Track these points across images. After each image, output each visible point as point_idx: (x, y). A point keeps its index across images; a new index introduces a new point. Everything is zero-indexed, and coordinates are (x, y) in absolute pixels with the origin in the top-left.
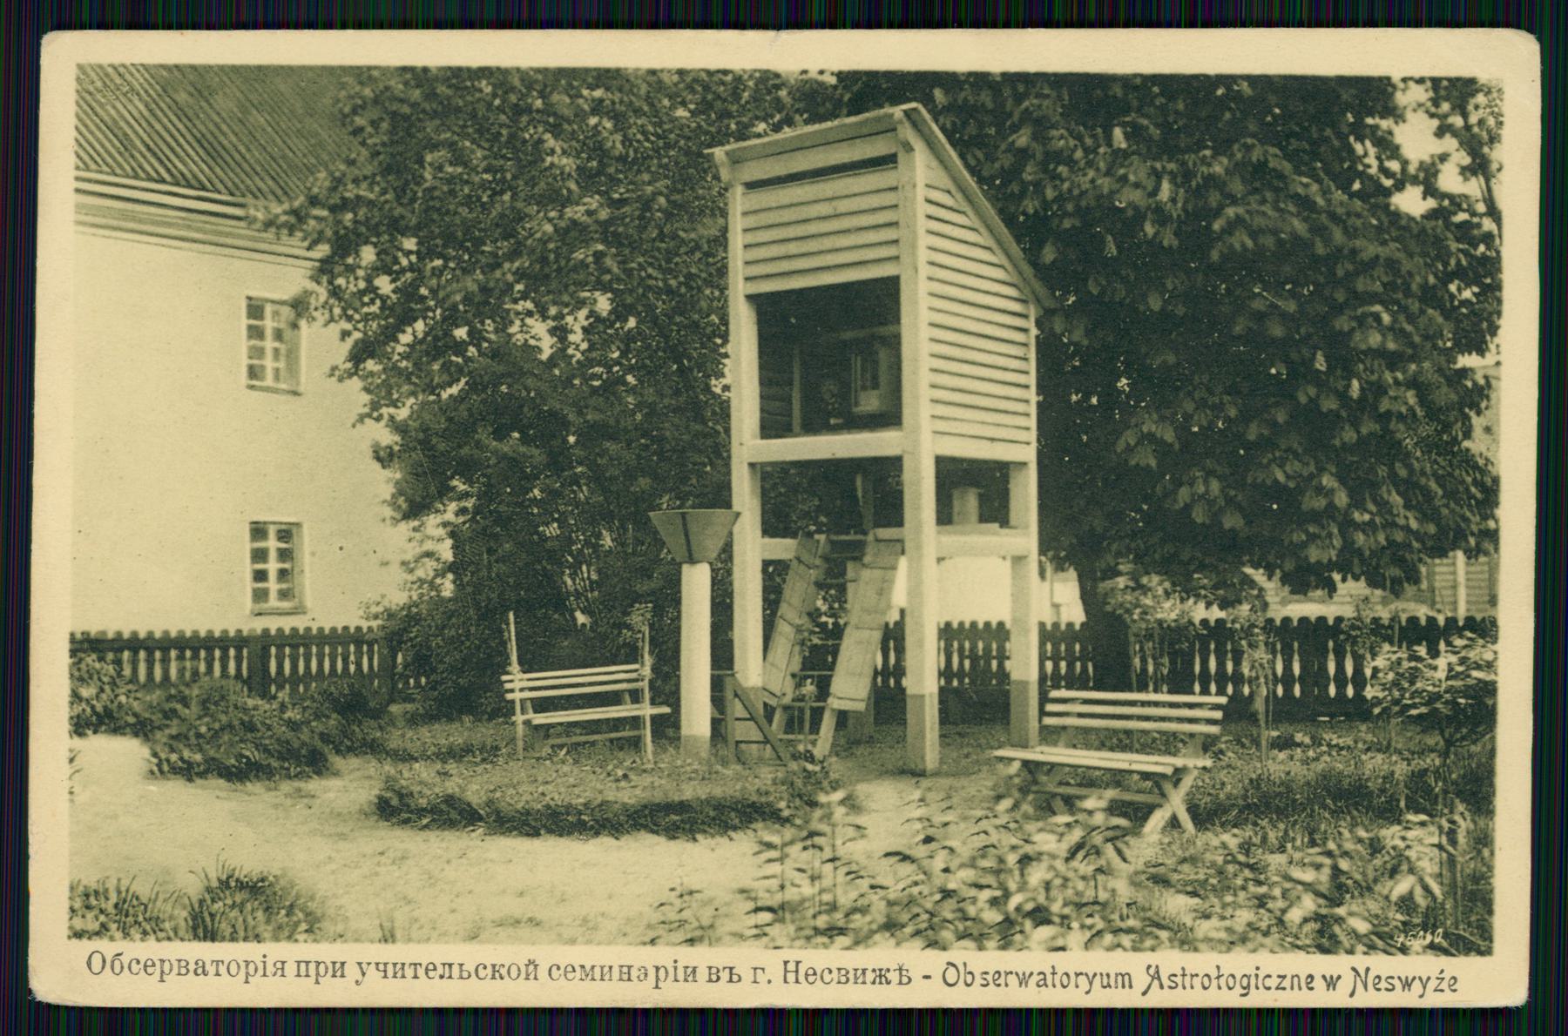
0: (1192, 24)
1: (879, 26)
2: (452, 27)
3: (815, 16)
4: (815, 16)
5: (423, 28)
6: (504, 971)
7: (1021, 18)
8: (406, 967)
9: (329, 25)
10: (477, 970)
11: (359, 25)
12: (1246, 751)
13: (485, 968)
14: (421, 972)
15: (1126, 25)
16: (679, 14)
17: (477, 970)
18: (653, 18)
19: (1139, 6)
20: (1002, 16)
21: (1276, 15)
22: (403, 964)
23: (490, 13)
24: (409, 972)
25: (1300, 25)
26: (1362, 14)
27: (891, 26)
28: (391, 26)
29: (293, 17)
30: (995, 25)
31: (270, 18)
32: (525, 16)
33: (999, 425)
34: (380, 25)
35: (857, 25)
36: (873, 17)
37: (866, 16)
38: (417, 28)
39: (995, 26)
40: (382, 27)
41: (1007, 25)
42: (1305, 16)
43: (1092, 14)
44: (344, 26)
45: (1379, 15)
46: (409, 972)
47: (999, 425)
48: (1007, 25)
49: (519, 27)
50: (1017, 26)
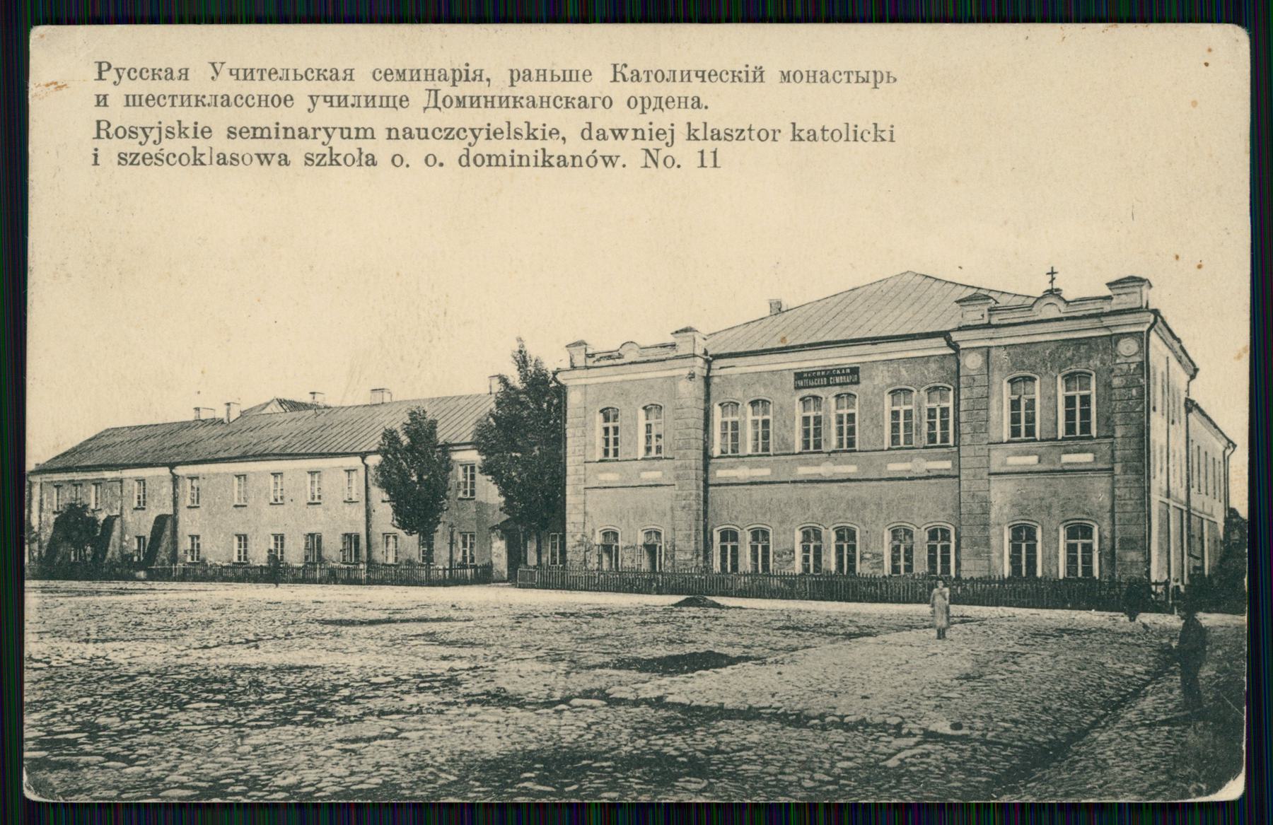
0: (881, 20)
1: (623, 21)
2: (271, 22)
3: (570, 13)
4: (570, 13)
5: (247, 23)
6: (340, 159)
7: (740, 15)
8: (255, 71)
9: (169, 20)
10: (306, 72)
11: (195, 20)
12: (740, 688)
13: (312, 72)
14: (266, 76)
15: (827, 21)
16: (458, 12)
17: (306, 72)
18: (437, 15)
19: (837, 6)
20: (724, 14)
21: (951, 13)
22: (252, 70)
23: (301, 10)
24: (257, 76)
25: (971, 21)
26: (1022, 13)
27: (633, 21)
28: (220, 21)
29: (139, 13)
30: (718, 21)
31: (120, 13)
32: (331, 14)
33: (656, 486)
34: (211, 20)
35: (605, 20)
36: (618, 12)
37: (612, 13)
38: (242, 23)
39: (719, 21)
40: (212, 22)
41: (729, 21)
42: (975, 14)
43: (798, 11)
44: (181, 21)
45: (1035, 12)
46: (257, 76)
47: (656, 486)
48: (729, 20)
49: (326, 22)
50: (738, 21)
